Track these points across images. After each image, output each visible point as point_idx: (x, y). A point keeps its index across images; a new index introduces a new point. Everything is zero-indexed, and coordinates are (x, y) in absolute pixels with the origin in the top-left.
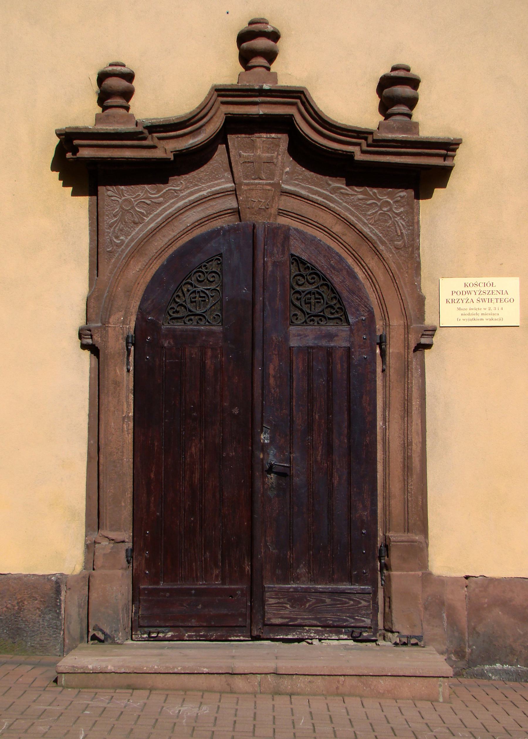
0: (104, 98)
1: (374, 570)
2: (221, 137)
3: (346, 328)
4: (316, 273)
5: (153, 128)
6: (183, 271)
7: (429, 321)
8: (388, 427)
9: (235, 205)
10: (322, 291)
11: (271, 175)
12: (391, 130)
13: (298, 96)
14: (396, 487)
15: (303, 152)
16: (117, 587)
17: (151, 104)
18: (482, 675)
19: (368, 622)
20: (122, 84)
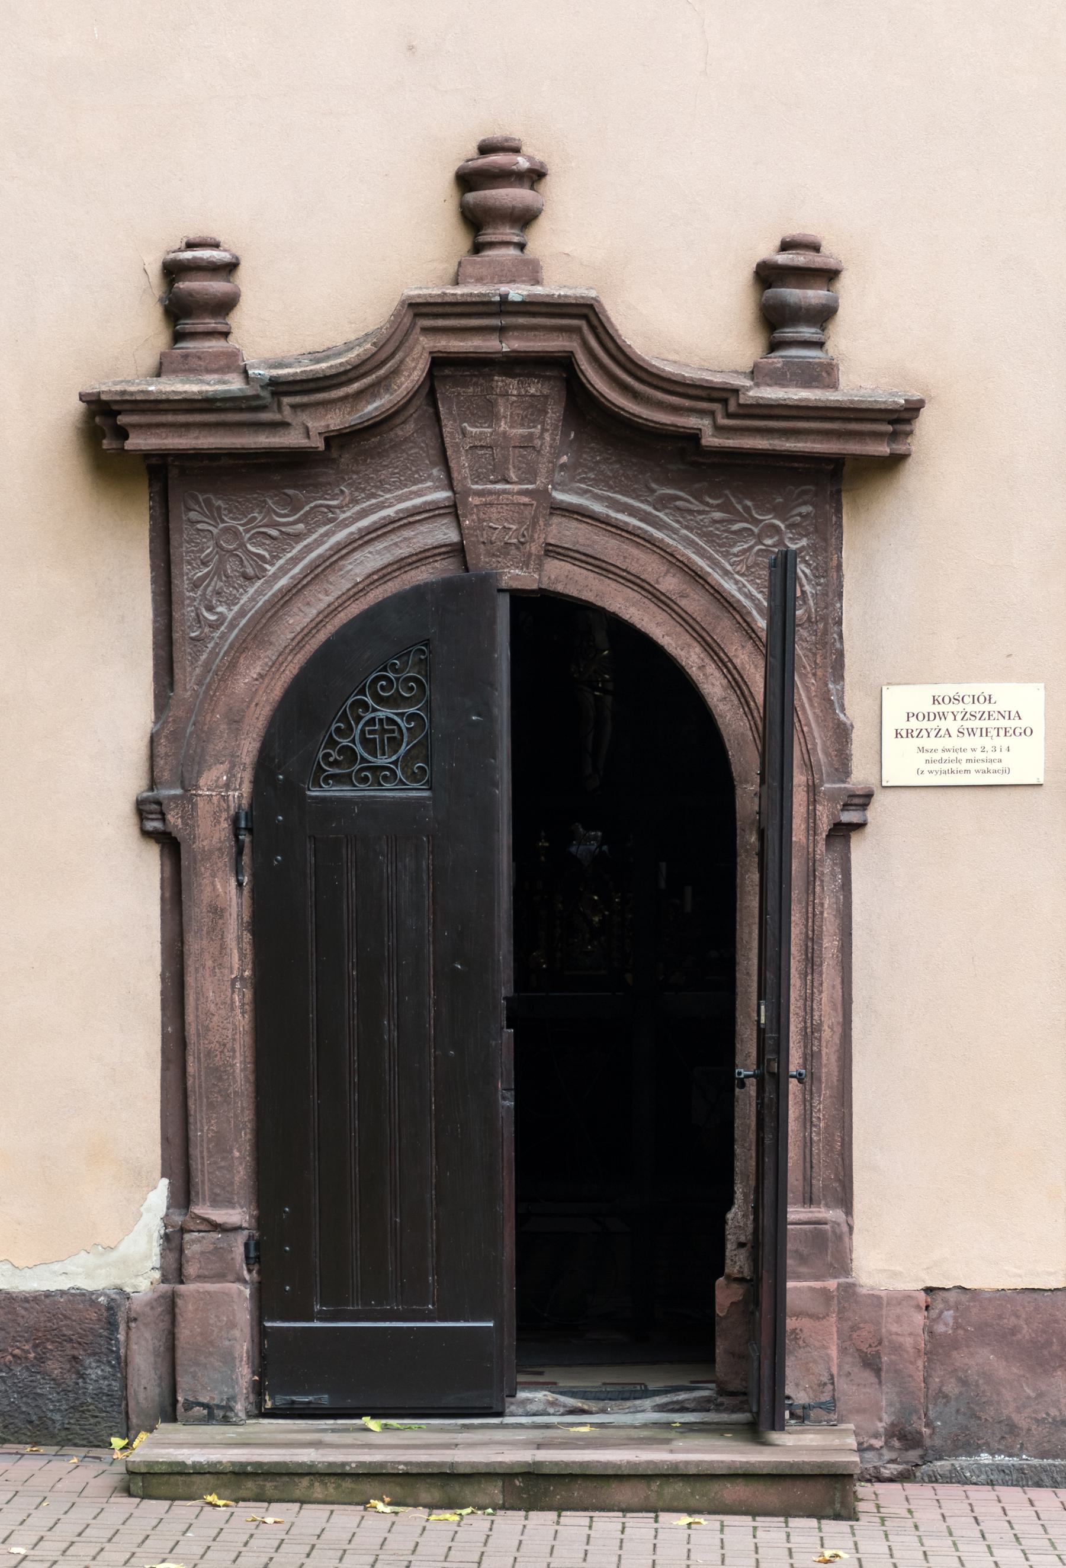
5: (279, 388)
7: (860, 776)
9: (453, 536)
11: (530, 474)
12: (778, 378)
13: (586, 315)
15: (590, 420)
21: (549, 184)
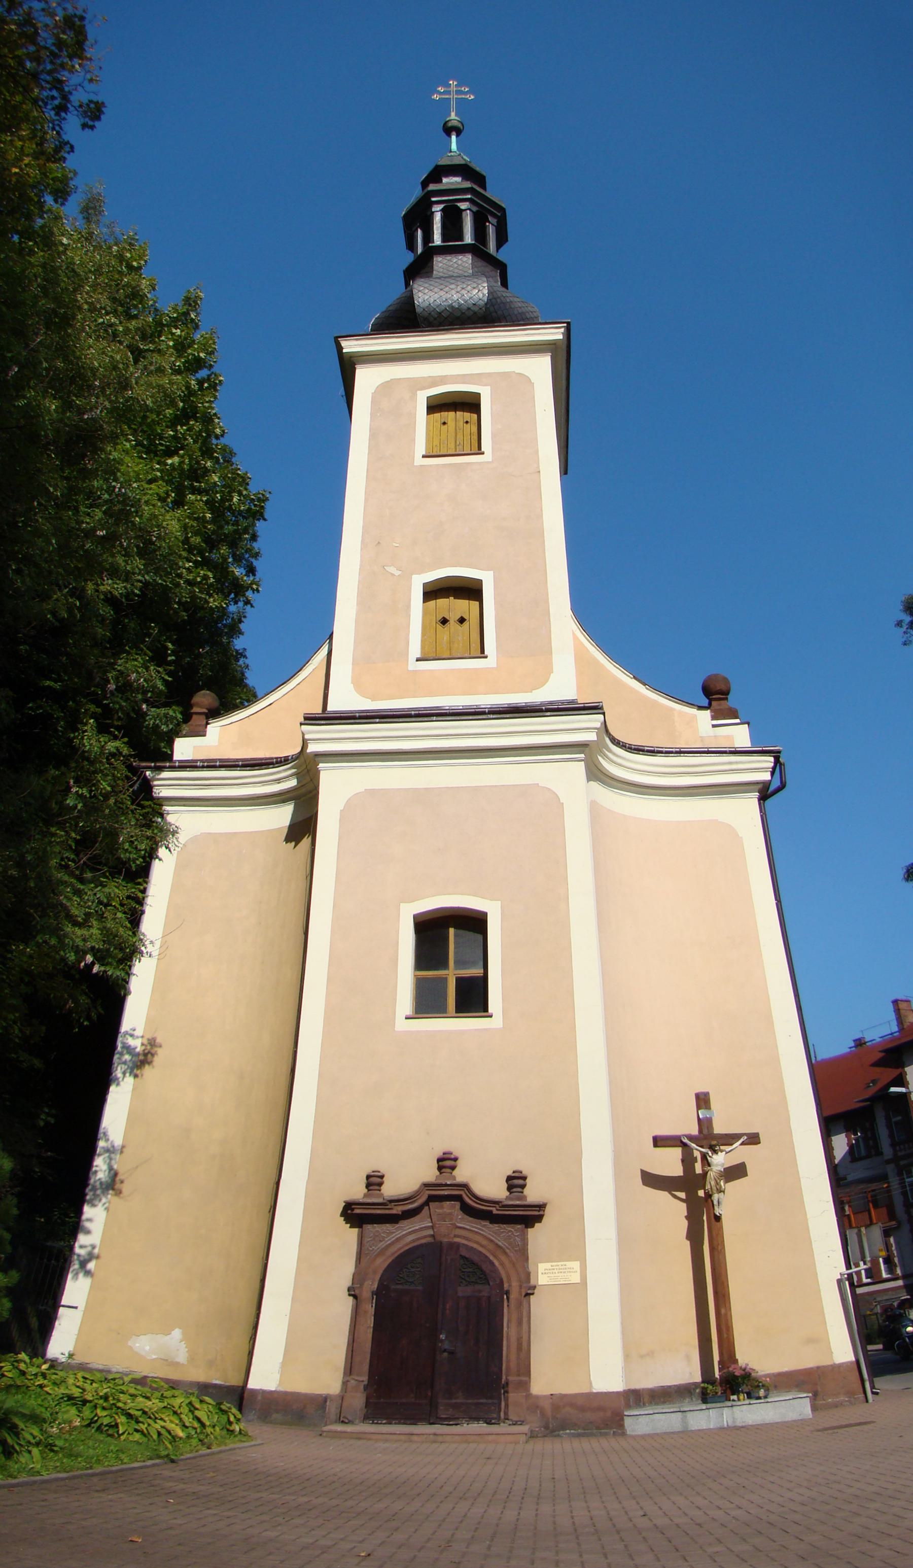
0: (368, 1186)
1: (500, 1394)
2: (426, 1203)
3: (487, 1286)
4: (473, 1263)
5: (391, 1201)
6: (402, 1263)
7: (532, 1282)
8: (509, 1331)
9: (432, 1233)
10: (477, 1270)
11: (451, 1220)
12: (511, 1199)
13: (465, 1186)
14: (513, 1357)
15: (467, 1210)
16: (358, 1400)
17: (390, 1189)
18: (559, 1436)
19: (495, 1416)
20: (379, 1180)
21: (458, 1162)
